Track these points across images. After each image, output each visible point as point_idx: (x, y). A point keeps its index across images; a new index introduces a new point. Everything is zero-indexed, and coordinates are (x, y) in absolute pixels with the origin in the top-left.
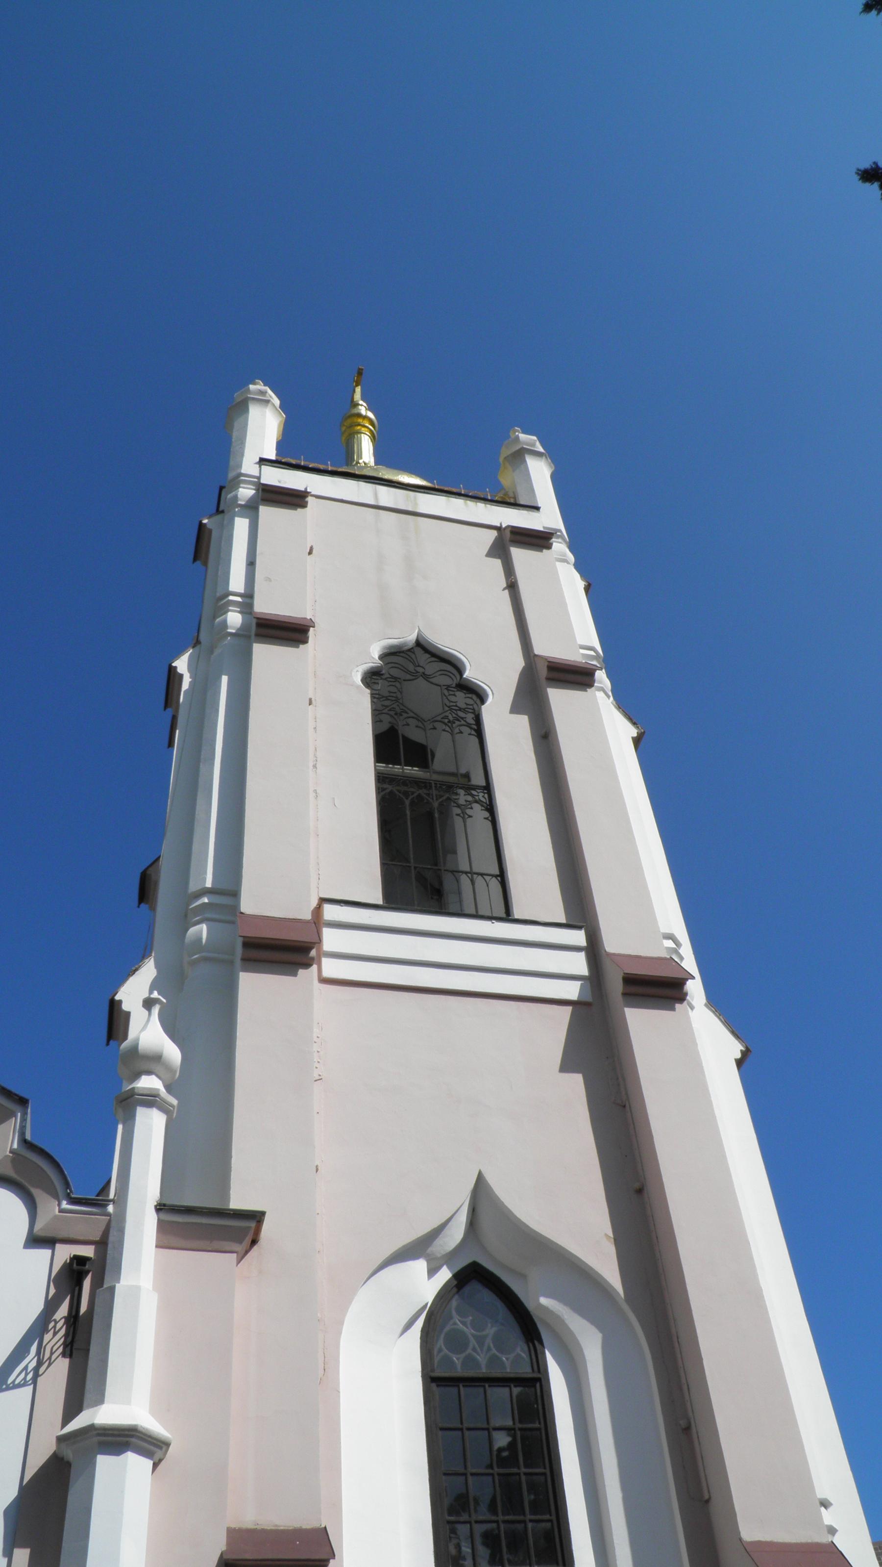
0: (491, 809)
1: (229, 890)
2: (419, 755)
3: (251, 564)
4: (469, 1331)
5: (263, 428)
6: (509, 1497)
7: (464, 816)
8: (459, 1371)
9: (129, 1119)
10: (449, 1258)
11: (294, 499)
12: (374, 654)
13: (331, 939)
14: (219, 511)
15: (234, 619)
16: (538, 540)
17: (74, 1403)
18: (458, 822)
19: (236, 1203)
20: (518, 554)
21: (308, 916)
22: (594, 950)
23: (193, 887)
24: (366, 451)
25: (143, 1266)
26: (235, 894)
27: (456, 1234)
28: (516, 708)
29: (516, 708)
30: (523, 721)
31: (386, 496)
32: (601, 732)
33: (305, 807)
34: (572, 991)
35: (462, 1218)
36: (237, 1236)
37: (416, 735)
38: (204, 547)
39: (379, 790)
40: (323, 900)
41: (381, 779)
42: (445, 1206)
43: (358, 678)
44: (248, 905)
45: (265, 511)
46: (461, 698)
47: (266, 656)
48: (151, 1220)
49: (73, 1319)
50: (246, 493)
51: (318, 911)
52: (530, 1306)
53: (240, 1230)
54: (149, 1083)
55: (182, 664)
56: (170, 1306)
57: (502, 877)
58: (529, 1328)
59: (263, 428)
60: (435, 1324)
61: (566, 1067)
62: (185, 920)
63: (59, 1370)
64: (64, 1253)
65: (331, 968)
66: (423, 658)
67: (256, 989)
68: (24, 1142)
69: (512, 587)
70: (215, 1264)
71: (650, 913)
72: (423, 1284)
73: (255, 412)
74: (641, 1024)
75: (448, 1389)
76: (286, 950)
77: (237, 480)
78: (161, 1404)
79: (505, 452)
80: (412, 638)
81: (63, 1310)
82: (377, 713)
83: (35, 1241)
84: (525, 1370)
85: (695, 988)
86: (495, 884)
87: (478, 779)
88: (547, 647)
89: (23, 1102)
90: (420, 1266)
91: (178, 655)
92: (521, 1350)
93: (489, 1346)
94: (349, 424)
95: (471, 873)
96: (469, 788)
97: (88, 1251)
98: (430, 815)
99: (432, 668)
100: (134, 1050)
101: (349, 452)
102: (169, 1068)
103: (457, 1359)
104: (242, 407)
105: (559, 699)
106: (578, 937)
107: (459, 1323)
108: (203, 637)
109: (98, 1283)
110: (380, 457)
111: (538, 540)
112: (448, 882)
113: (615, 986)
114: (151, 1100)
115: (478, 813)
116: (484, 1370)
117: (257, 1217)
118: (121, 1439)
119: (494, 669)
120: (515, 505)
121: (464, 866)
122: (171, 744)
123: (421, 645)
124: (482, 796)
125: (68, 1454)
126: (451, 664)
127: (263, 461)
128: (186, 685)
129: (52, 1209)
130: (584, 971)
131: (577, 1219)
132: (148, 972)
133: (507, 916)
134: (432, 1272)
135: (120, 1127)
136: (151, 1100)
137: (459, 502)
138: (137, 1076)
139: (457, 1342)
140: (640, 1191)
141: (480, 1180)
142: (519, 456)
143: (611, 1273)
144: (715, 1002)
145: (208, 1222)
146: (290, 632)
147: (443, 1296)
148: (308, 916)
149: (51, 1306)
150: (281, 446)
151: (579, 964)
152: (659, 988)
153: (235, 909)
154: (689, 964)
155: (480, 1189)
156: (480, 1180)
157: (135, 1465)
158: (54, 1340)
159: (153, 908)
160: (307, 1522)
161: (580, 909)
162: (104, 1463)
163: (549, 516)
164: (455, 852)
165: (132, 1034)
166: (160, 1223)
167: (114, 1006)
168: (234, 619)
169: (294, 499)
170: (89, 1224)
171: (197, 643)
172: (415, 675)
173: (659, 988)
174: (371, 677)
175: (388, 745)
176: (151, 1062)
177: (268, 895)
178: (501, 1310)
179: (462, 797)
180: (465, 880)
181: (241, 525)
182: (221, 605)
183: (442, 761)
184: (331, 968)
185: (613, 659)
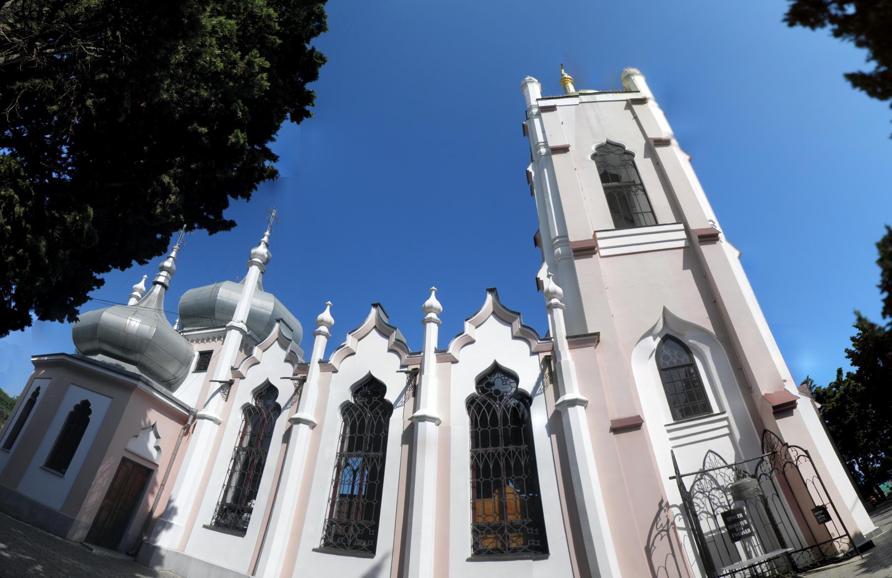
0: (644, 190)
1: (564, 235)
2: (616, 178)
3: (544, 132)
4: (669, 354)
5: (534, 90)
6: (691, 397)
7: (636, 195)
8: (669, 366)
9: (552, 313)
10: (659, 335)
11: (552, 108)
12: (593, 149)
13: (601, 243)
14: (527, 119)
15: (543, 150)
16: (643, 101)
17: (557, 395)
18: (634, 197)
19: (590, 331)
20: (635, 107)
21: (591, 238)
22: (687, 229)
23: (553, 237)
24: (571, 88)
25: (568, 357)
26: (567, 236)
27: (660, 326)
28: (645, 157)
29: (645, 157)
30: (649, 160)
31: (584, 98)
32: (677, 159)
33: (583, 203)
34: (682, 244)
35: (661, 321)
36: (592, 341)
37: (614, 172)
38: (526, 131)
39: (605, 192)
40: (595, 232)
41: (605, 188)
42: (655, 319)
43: (589, 158)
44: (572, 239)
45: (543, 115)
46: (626, 157)
47: (556, 158)
48: (565, 342)
49: (551, 373)
50: (535, 111)
51: (594, 235)
52: (686, 343)
53: (593, 339)
54: (554, 301)
55: (530, 169)
56: (577, 364)
57: (652, 212)
58: (687, 350)
59: (534, 90)
60: (659, 355)
61: (685, 268)
62: (553, 248)
63: (550, 388)
64: (542, 355)
65: (603, 252)
66: (610, 147)
67: (581, 265)
68: (522, 325)
69: (636, 118)
70: (588, 351)
71: (703, 213)
72: (653, 343)
73: (530, 86)
74: (706, 250)
75: (665, 371)
76: (587, 250)
77: (531, 108)
78: (582, 392)
79: (623, 76)
80: (605, 141)
81: (547, 371)
82: (599, 168)
83: (533, 353)
84: (689, 362)
85: (721, 236)
86: (650, 214)
87: (638, 182)
88: (652, 135)
89: (519, 314)
90: (651, 338)
91: (528, 166)
92: (686, 357)
93: (676, 357)
94: (563, 82)
95: (642, 213)
96: (635, 185)
97: (549, 354)
98: (624, 196)
99: (614, 149)
100: (548, 291)
101: (565, 90)
102: (559, 295)
103: (668, 363)
104: (525, 85)
105: (660, 151)
106: (681, 226)
107: (666, 352)
108: (534, 158)
109: (555, 361)
110: (576, 89)
111: (643, 101)
112: (635, 217)
113: (696, 239)
114: (556, 306)
115: (640, 193)
116: (676, 364)
117: (598, 334)
118: (573, 403)
119: (635, 145)
120: (631, 92)
121: (639, 211)
122: (532, 194)
123: (608, 143)
124: (640, 187)
125: (559, 409)
126: (620, 147)
127: (537, 100)
128: (533, 175)
129: (535, 344)
130: (685, 237)
131: (696, 313)
132: (545, 267)
133: (657, 224)
134: (655, 339)
135: (549, 316)
136: (556, 306)
137: (610, 95)
138: (550, 299)
139: (666, 358)
140: (715, 302)
141: (664, 308)
142: (629, 76)
143: (709, 327)
144: (729, 239)
145: (583, 339)
146: (564, 149)
147: (659, 345)
148: (591, 238)
149: (543, 371)
150: (542, 93)
151: (683, 235)
152: (710, 238)
153: (567, 241)
154: (719, 228)
155: (665, 311)
156: (664, 308)
157: (579, 409)
158: (547, 380)
159: (541, 247)
160: (633, 414)
161: (680, 217)
162: (570, 410)
163: (645, 91)
164: (635, 207)
165: (545, 287)
166: (569, 343)
167: (537, 279)
168: (543, 150)
169: (552, 108)
170: (547, 346)
171: (532, 161)
172: (609, 153)
173: (710, 238)
174: (594, 157)
175: (605, 177)
176: (553, 294)
177: (577, 234)
178: (678, 347)
179: (634, 189)
180: (640, 215)
181: (537, 121)
182: (538, 147)
183: (624, 178)
184: (603, 252)
185: (676, 136)
